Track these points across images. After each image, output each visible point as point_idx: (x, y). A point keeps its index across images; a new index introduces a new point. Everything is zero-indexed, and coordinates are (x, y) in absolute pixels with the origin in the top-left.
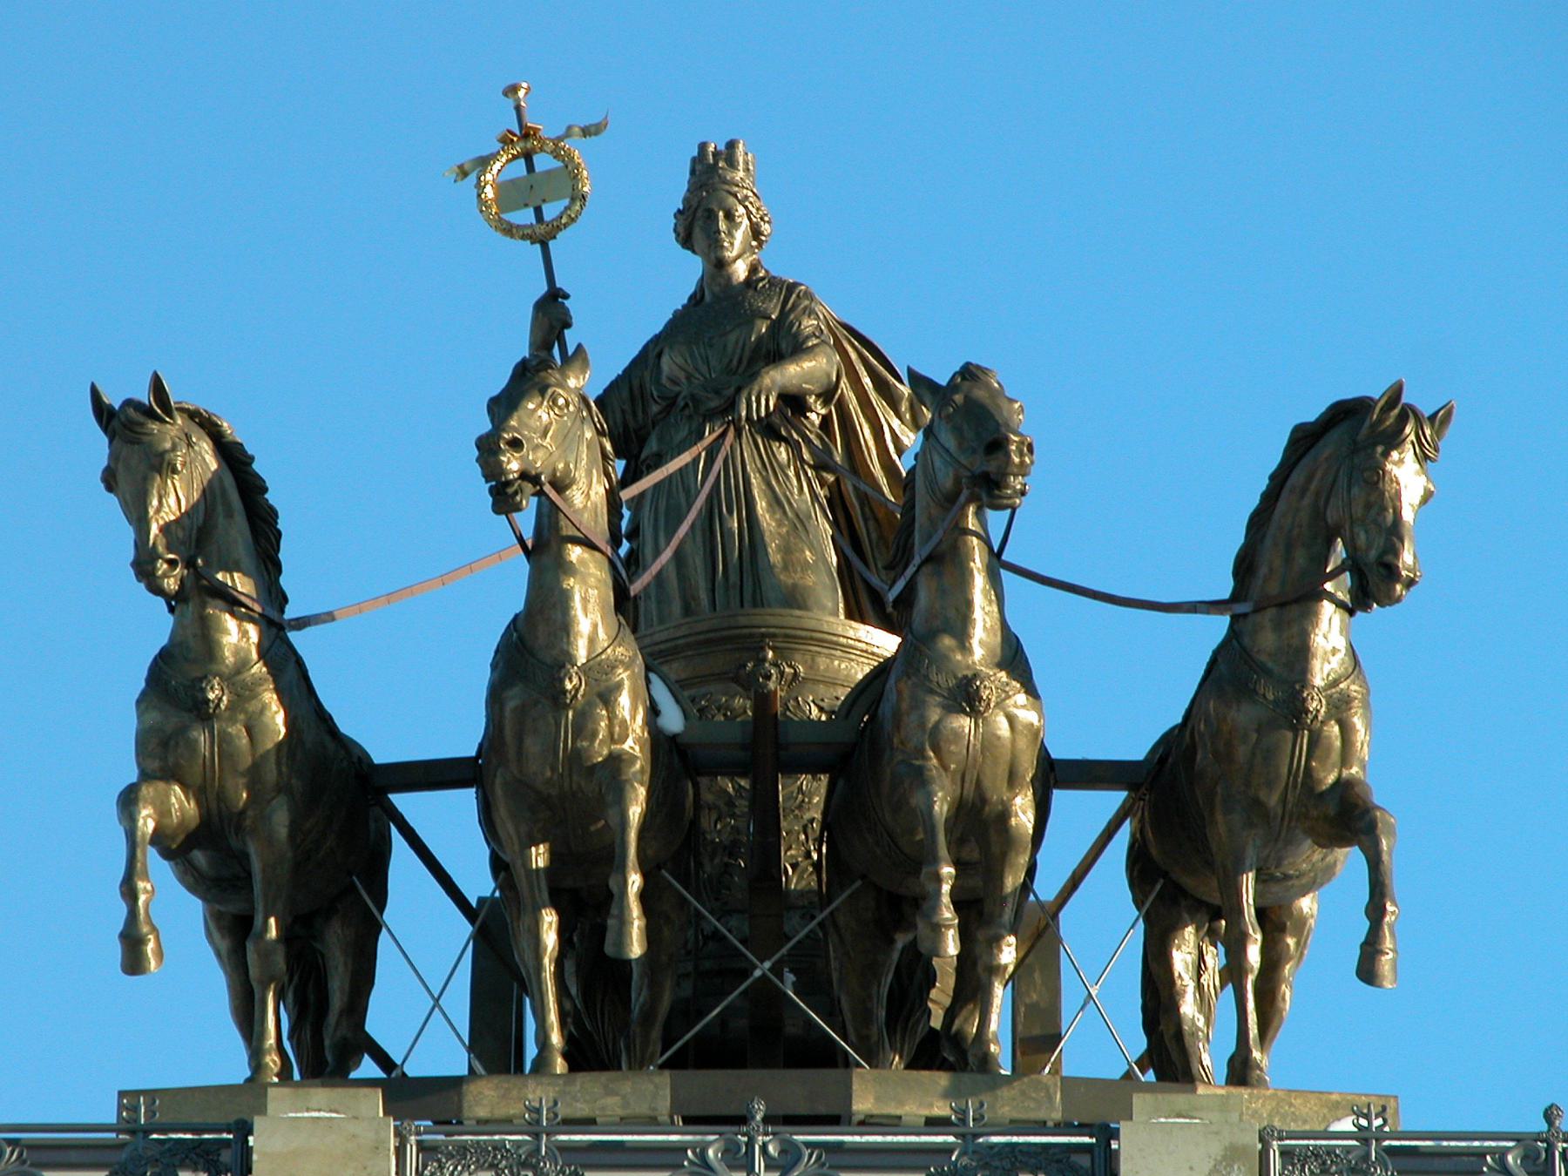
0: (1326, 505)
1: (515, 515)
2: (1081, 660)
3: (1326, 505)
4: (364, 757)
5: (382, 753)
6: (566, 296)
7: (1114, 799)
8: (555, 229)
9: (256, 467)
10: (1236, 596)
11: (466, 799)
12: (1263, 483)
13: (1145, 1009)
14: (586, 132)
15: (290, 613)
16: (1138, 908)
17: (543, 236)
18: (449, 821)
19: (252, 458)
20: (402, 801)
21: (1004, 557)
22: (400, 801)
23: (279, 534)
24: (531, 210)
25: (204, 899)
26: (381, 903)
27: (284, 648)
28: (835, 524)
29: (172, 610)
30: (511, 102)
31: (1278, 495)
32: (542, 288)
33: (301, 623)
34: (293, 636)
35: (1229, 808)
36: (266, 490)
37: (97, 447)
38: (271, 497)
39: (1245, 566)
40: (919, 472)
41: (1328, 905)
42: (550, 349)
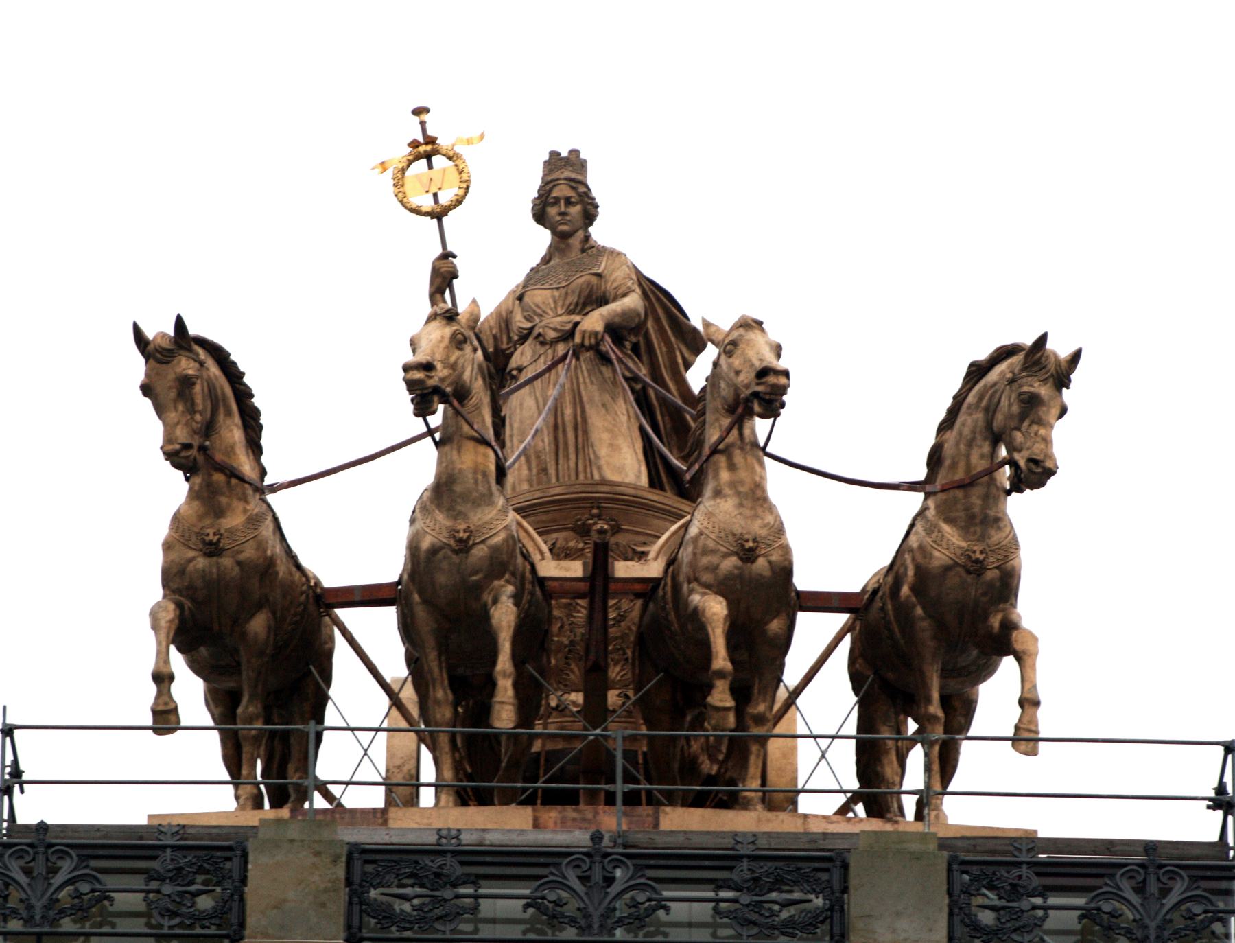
0: (1005, 415)
1: (428, 418)
2: (840, 527)
3: (1005, 415)
4: (318, 583)
5: (330, 579)
6: (454, 257)
7: (842, 618)
8: (446, 211)
9: (246, 380)
10: (930, 479)
11: (388, 616)
12: (948, 402)
13: (858, 763)
14: (469, 142)
15: (268, 481)
16: (857, 695)
17: (438, 215)
18: (378, 630)
19: (243, 374)
20: (343, 613)
21: (768, 450)
22: (342, 613)
23: (261, 427)
24: (430, 196)
25: (205, 679)
26: (328, 680)
27: (264, 506)
28: (552, 438)
29: (187, 479)
30: (416, 119)
31: (959, 410)
32: (439, 251)
33: (274, 489)
34: (270, 498)
35: (938, 634)
36: (252, 396)
37: (137, 367)
38: (256, 401)
39: (935, 459)
40: (708, 389)
41: (996, 698)
42: (443, 293)
